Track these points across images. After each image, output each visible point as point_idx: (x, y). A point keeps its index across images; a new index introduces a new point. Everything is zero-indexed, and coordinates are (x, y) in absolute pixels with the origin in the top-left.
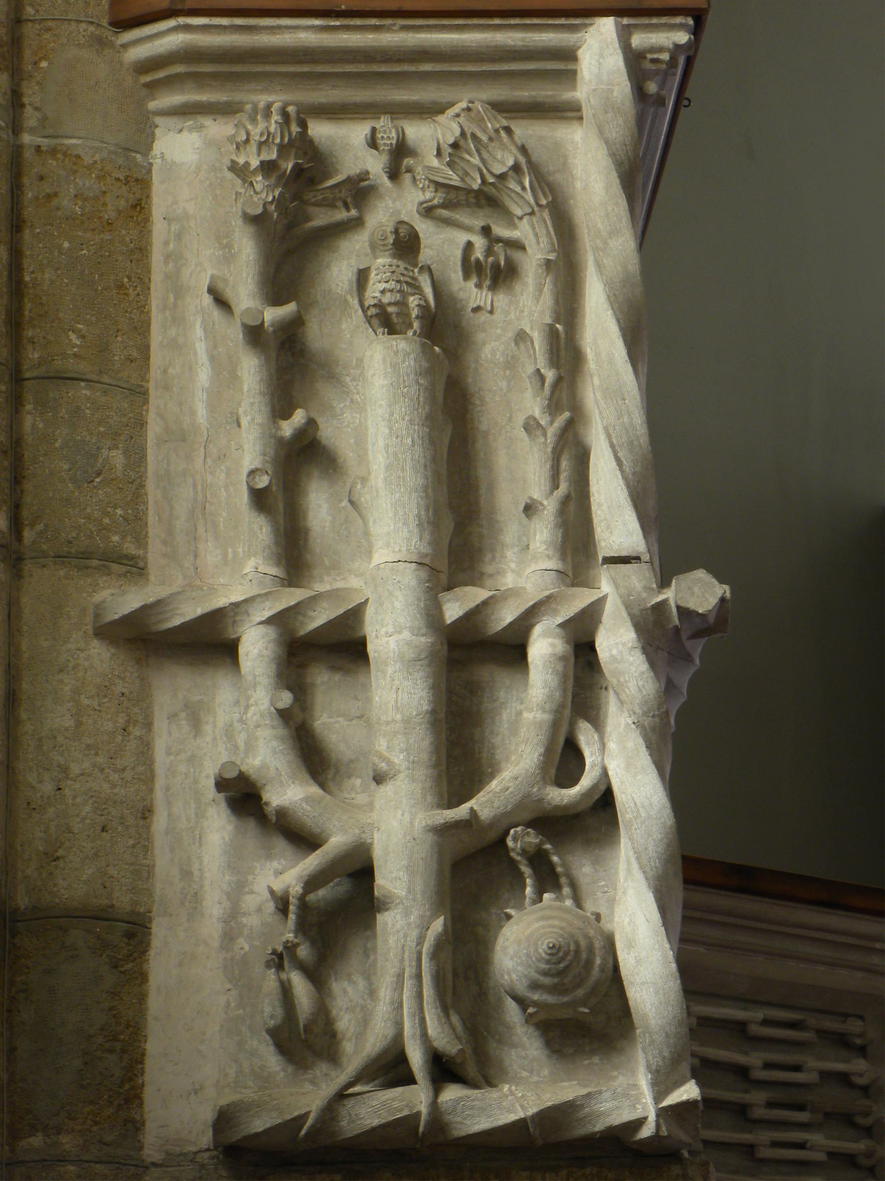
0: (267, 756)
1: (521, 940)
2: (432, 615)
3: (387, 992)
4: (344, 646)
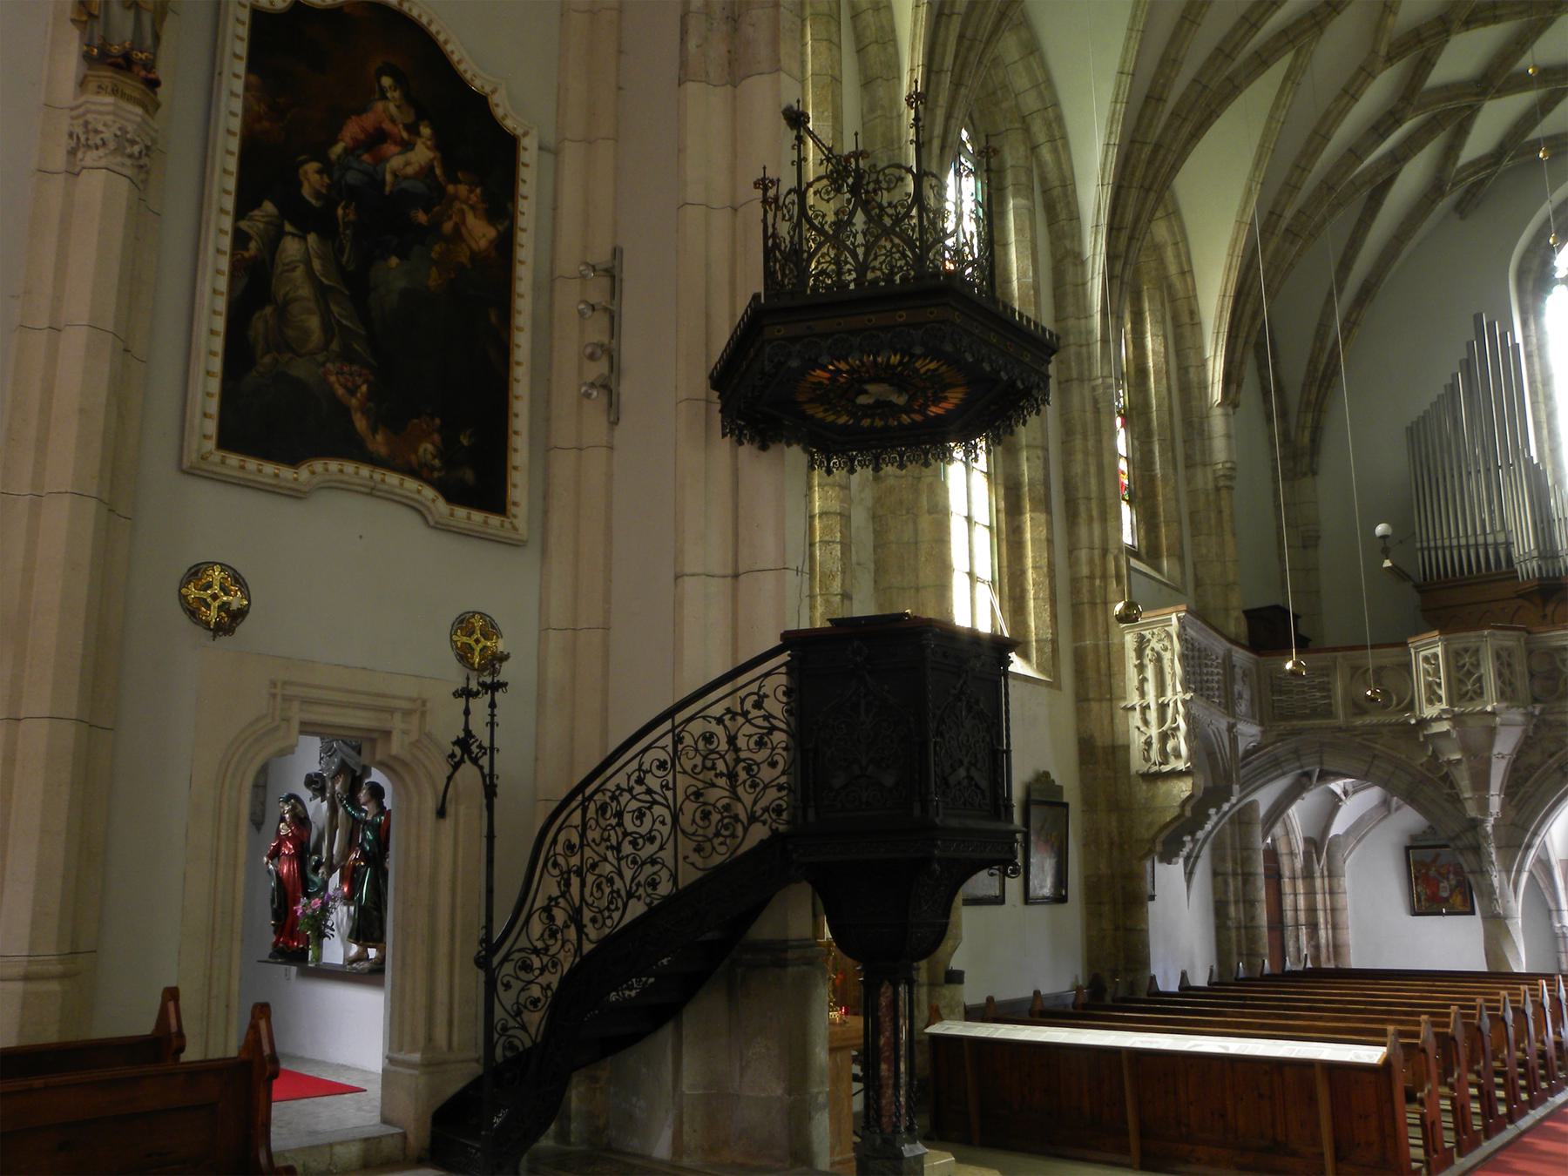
0: (1140, 724)
3: (1155, 754)
4: (1148, 707)
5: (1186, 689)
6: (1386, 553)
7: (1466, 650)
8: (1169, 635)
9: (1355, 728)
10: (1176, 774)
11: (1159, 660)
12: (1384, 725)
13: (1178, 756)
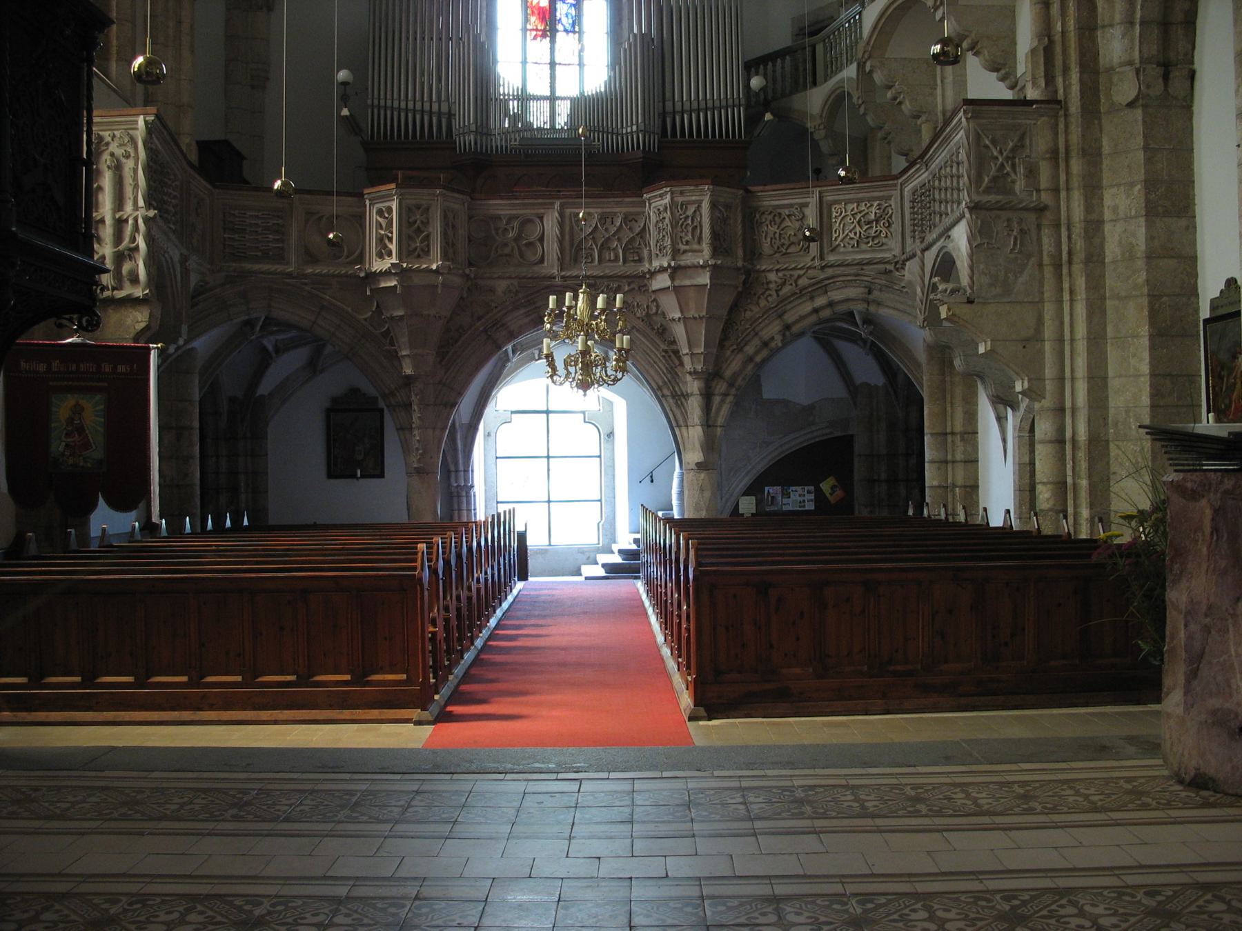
1: (126, 267)
2: (114, 218)
5: (149, 205)
6: (344, 100)
7: (418, 207)
8: (133, 140)
9: (306, 276)
10: (131, 301)
11: (118, 168)
12: (333, 276)
13: (134, 280)
